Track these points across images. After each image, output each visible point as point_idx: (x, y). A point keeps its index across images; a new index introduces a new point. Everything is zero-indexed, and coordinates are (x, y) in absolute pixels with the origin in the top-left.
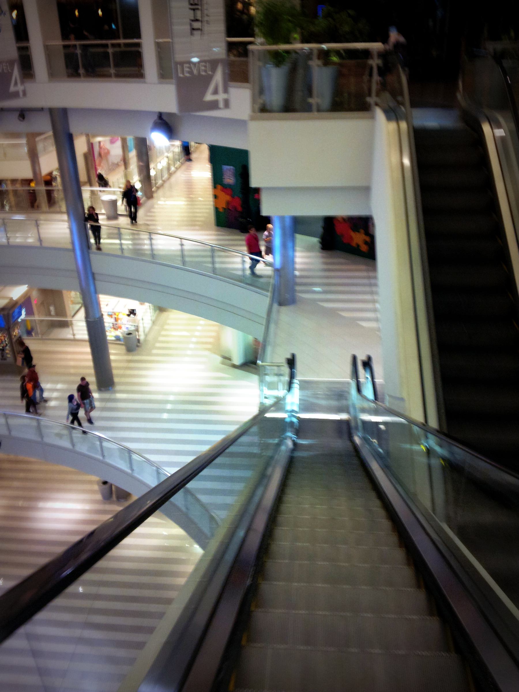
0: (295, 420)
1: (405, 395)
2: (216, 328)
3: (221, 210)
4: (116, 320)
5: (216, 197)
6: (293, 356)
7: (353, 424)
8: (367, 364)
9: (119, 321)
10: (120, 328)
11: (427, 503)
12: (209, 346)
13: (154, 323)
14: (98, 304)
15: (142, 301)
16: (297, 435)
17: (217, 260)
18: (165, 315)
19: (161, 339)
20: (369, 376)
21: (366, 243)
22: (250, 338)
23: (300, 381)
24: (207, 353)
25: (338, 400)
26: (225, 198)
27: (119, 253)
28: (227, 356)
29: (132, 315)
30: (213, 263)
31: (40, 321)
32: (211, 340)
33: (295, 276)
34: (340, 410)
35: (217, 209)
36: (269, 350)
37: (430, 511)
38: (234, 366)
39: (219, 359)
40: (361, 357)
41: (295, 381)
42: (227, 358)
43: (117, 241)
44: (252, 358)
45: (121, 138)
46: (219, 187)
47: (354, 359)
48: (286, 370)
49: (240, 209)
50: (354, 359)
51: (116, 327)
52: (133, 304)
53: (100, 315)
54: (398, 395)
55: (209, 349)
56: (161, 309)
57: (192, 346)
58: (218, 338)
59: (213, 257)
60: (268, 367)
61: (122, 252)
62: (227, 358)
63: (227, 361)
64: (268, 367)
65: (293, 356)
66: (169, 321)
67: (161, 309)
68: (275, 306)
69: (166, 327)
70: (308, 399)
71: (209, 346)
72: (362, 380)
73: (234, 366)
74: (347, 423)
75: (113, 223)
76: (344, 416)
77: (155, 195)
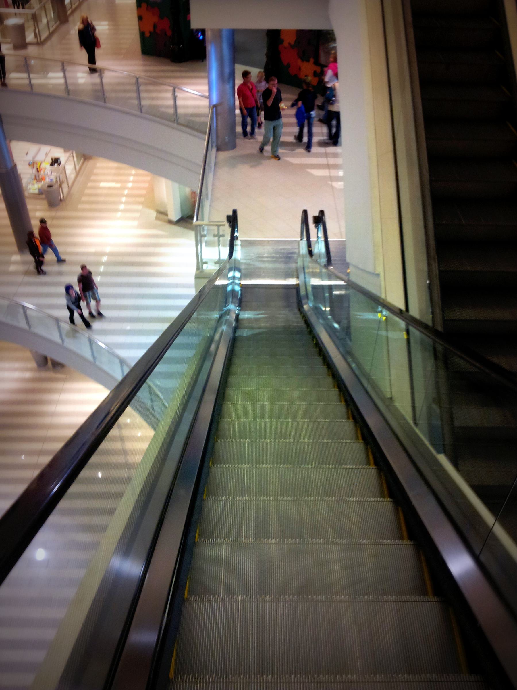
0: (237, 288)
1: (380, 270)
2: (148, 178)
3: (147, 35)
4: (38, 170)
5: (140, 18)
6: (235, 212)
7: (303, 292)
8: (319, 220)
9: (42, 172)
10: (43, 179)
11: (406, 411)
12: (142, 199)
13: (78, 174)
14: (10, 153)
15: (66, 148)
16: (239, 306)
17: (143, 95)
18: (90, 164)
19: (87, 191)
20: (321, 234)
21: (315, 74)
22: (187, 191)
23: (242, 241)
24: (140, 207)
25: (286, 263)
26: (152, 19)
27: (28, 89)
28: (162, 210)
29: (56, 165)
30: (139, 99)
31: (29, 164)
32: (144, 192)
33: (218, 465)
34: (288, 275)
35: (142, 34)
36: (207, 204)
37: (411, 421)
38: (170, 222)
39: (154, 214)
40: (313, 213)
41: (238, 242)
42: (162, 213)
43: (25, 75)
44: (188, 212)
45: (345, 240)
46: (144, 5)
47: (305, 212)
48: (227, 230)
49: (169, 33)
50: (305, 212)
51: (37, 178)
52: (58, 153)
53: (13, 165)
54: (370, 269)
55: (139, 203)
56: (85, 157)
57: (124, 199)
58: (151, 190)
59: (138, 91)
60: (206, 227)
61: (32, 88)
62: (162, 213)
63: (162, 217)
64: (206, 227)
65: (235, 212)
66: (95, 171)
67: (85, 157)
68: (213, 152)
69: (93, 178)
70: (252, 263)
71: (142, 199)
72: (313, 239)
73: (170, 222)
74: (297, 287)
75: (22, 52)
76: (293, 281)
77: (71, 19)
